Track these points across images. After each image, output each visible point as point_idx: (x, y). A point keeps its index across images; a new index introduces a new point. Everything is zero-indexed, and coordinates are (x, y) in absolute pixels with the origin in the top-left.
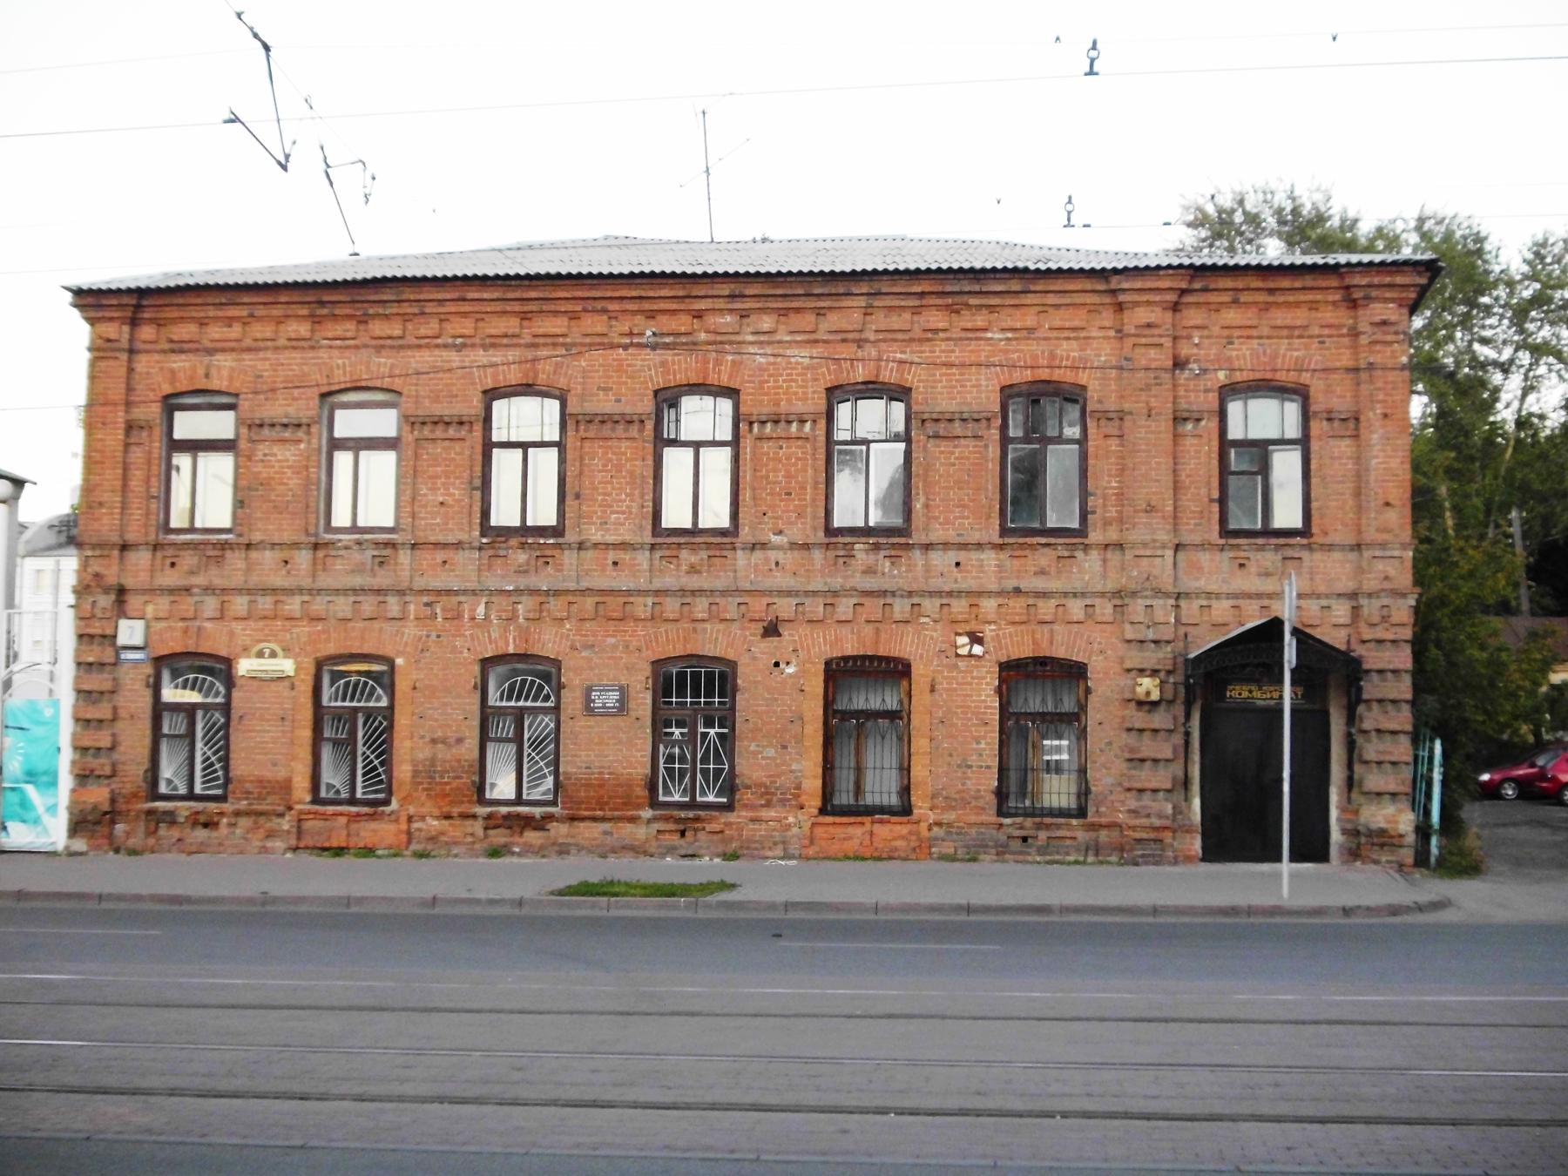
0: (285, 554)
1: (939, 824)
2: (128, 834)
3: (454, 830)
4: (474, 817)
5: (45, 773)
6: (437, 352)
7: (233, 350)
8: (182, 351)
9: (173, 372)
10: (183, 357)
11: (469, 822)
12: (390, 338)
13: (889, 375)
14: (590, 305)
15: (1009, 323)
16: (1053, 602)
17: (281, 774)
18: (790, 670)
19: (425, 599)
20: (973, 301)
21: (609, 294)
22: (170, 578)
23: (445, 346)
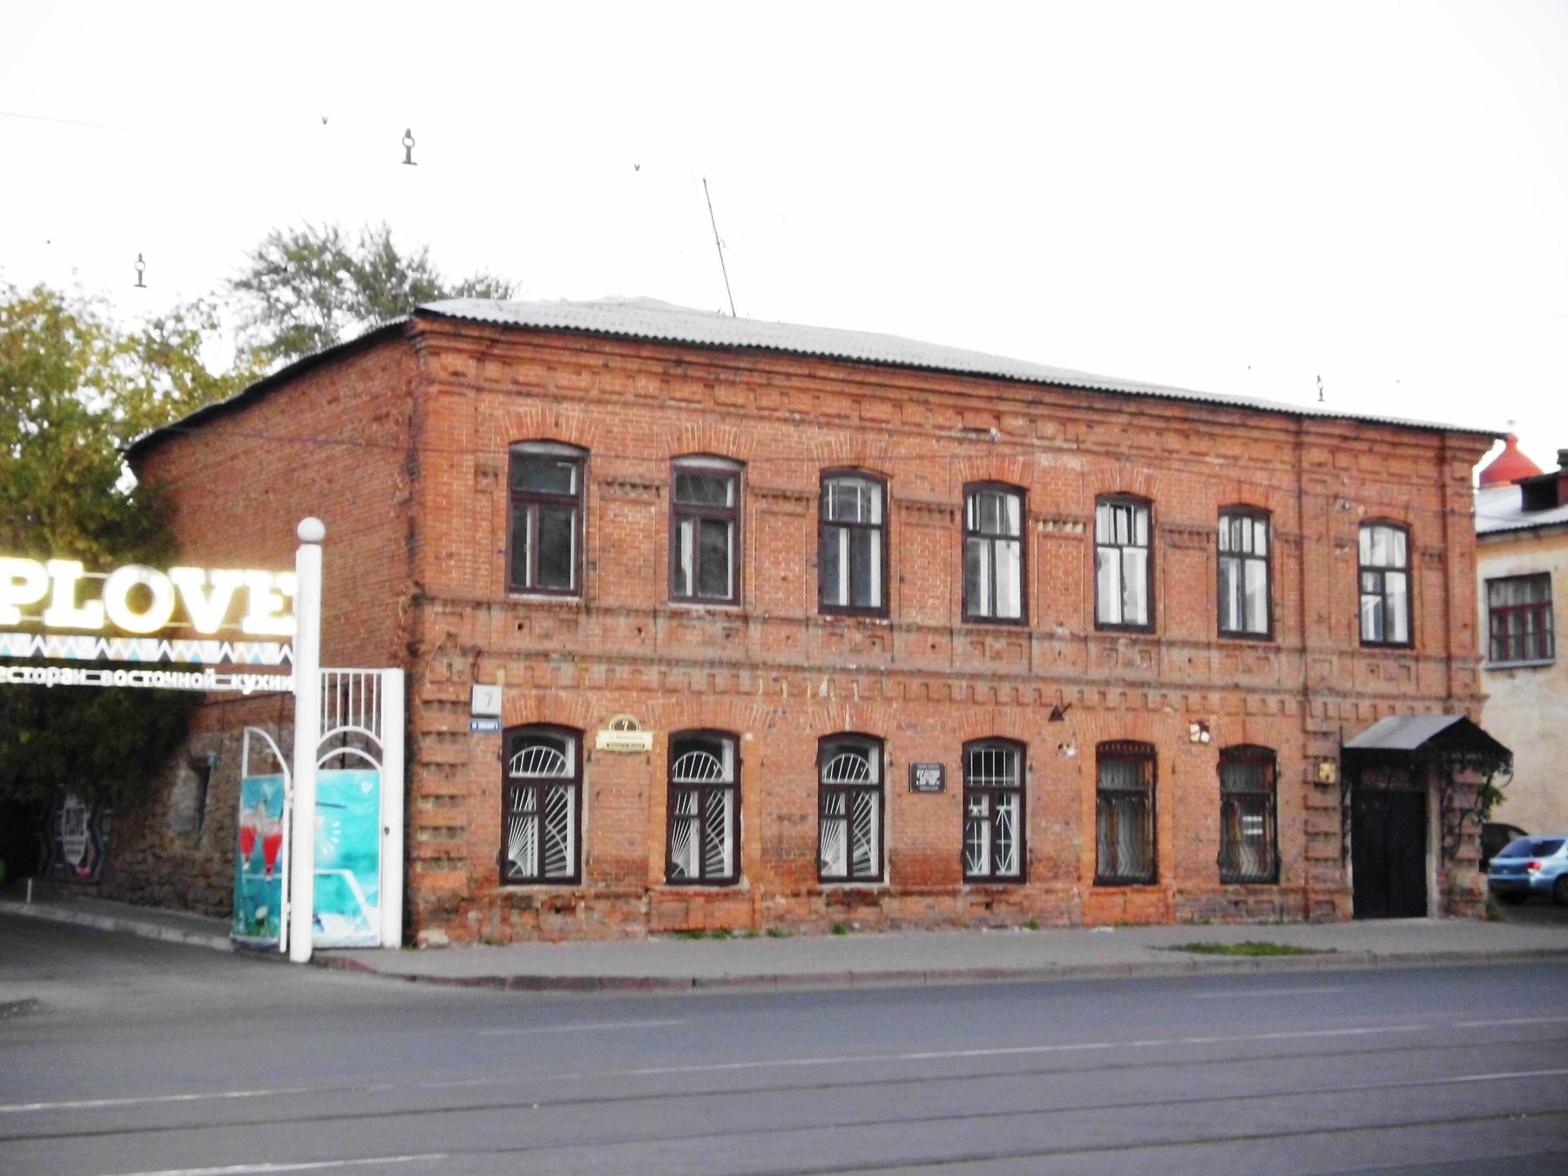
0: (640, 621)
1: (1180, 892)
2: (480, 922)
3: (799, 908)
4: (820, 894)
5: (364, 857)
6: (776, 425)
7: (581, 400)
8: (529, 395)
9: (518, 415)
10: (529, 401)
11: (814, 899)
12: (734, 405)
13: (1139, 488)
14: (915, 395)
15: (1223, 451)
16: (1257, 697)
17: (638, 853)
18: (1071, 752)
19: (774, 674)
20: (1203, 428)
21: (937, 387)
22: (523, 642)
23: (786, 420)
